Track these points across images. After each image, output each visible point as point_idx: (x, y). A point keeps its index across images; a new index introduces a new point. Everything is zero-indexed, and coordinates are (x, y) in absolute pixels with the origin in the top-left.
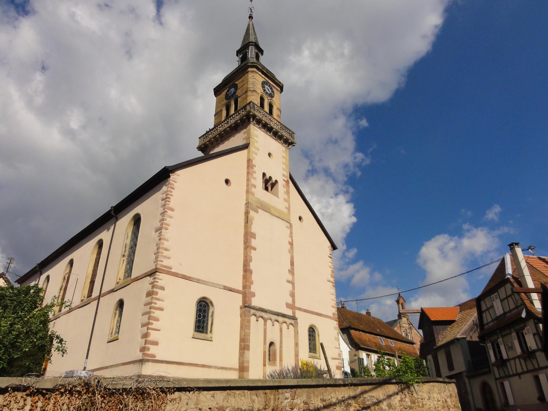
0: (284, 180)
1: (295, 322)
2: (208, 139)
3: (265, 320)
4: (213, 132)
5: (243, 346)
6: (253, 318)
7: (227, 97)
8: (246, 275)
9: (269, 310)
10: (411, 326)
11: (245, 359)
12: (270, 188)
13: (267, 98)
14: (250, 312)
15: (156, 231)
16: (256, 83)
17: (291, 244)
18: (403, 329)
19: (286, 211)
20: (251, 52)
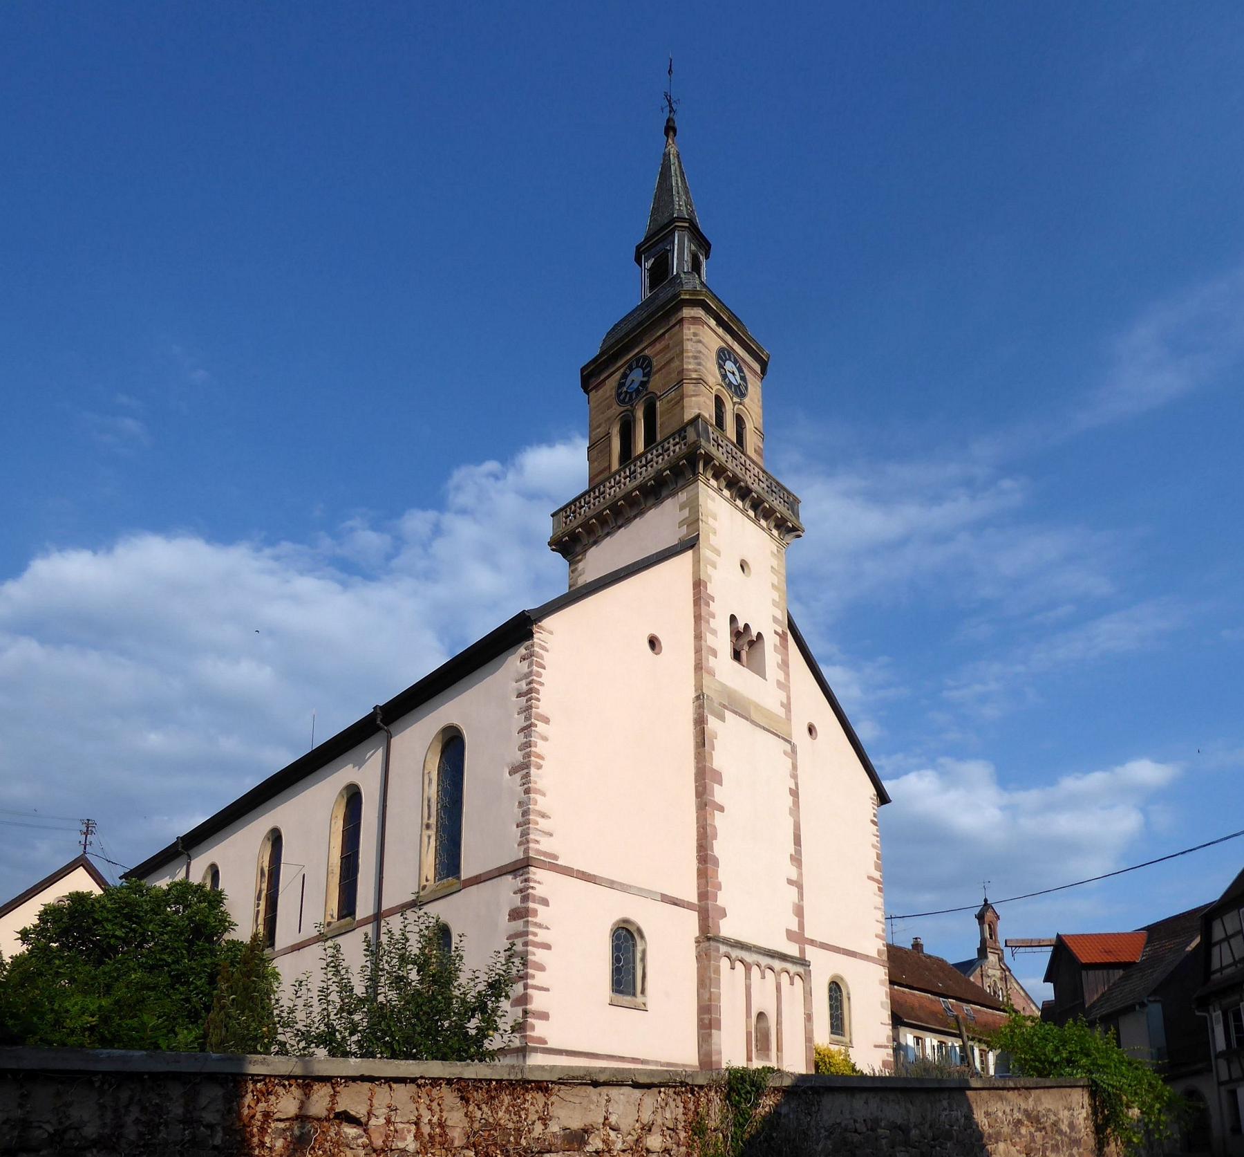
0: (776, 633)
1: (805, 970)
2: (579, 520)
3: (748, 967)
4: (592, 501)
5: (707, 1022)
6: (725, 963)
7: (625, 397)
8: (707, 868)
9: (754, 946)
10: (1007, 973)
11: (714, 1047)
12: (744, 654)
13: (732, 399)
14: (718, 950)
15: (513, 771)
16: (704, 354)
17: (795, 793)
18: (988, 980)
19: (781, 712)
20: (681, 250)
